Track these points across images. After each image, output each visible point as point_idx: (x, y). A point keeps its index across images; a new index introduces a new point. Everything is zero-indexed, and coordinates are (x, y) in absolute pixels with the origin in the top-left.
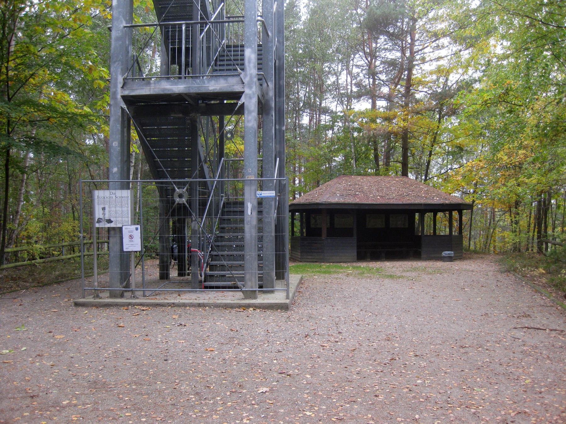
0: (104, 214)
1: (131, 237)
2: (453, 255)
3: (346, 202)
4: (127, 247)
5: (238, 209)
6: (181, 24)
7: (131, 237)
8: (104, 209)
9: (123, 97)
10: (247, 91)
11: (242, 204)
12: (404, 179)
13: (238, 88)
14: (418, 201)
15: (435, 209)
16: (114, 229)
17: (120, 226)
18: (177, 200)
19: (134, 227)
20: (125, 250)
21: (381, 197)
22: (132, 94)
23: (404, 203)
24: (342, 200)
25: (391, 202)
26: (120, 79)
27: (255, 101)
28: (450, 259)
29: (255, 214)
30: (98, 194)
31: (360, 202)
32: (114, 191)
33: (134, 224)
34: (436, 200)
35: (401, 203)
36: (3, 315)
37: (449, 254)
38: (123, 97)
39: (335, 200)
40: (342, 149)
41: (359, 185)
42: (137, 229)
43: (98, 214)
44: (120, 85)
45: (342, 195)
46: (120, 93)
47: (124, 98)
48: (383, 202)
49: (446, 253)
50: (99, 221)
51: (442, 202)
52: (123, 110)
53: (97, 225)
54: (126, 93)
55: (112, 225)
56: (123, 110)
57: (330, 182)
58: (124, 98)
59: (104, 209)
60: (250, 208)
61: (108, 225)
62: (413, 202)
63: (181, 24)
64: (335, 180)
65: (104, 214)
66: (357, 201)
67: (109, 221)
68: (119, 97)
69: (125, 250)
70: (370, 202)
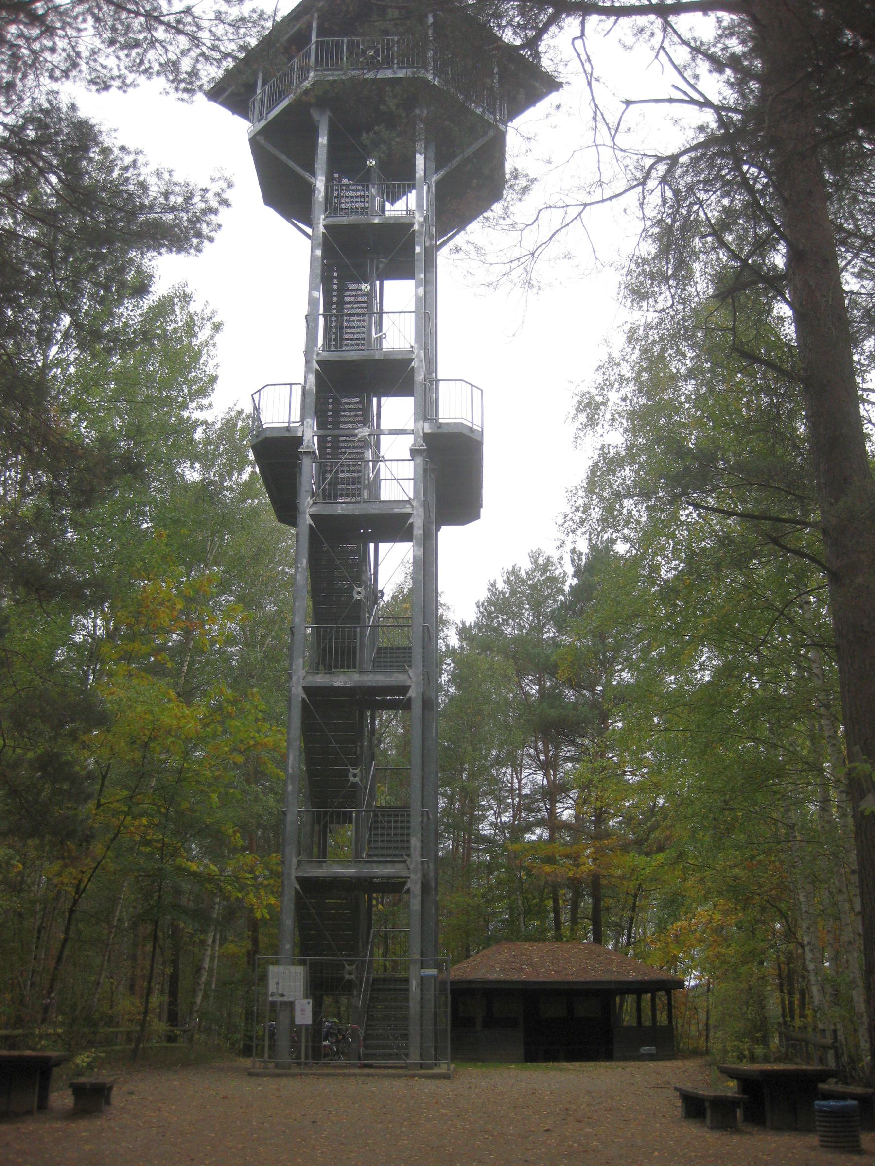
0: (277, 988)
1: (303, 1011)
2: (654, 1052)
3: (509, 979)
4: (298, 1021)
5: (404, 987)
6: (351, 813)
7: (303, 1011)
8: (277, 983)
9: (296, 878)
10: (413, 877)
11: (407, 981)
12: (595, 947)
13: (404, 873)
14: (607, 977)
15: (638, 988)
16: (285, 1003)
17: (292, 999)
18: (347, 977)
19: (307, 1001)
20: (297, 1022)
21: (557, 972)
22: (305, 875)
23: (588, 980)
24: (502, 977)
25: (571, 978)
26: (295, 861)
27: (419, 885)
28: (652, 1057)
29: (419, 990)
30: (272, 968)
31: (527, 980)
32: (288, 967)
33: (307, 998)
34: (632, 976)
35: (582, 980)
36: (4, 1127)
37: (649, 1050)
38: (296, 878)
39: (494, 977)
40: (504, 897)
41: (526, 955)
42: (309, 1003)
43: (272, 988)
44: (294, 867)
45: (503, 970)
46: (294, 874)
47: (298, 879)
48: (558, 979)
49: (645, 1049)
50: (272, 995)
51: (639, 978)
52: (296, 890)
53: (270, 999)
54: (300, 874)
55: (285, 999)
56: (296, 890)
57: (485, 952)
58: (298, 879)
59: (277, 983)
60: (414, 984)
61: (281, 999)
62: (599, 978)
63: (351, 813)
64: (494, 948)
65: (277, 988)
66: (523, 977)
67: (282, 995)
68: (293, 877)
69: (297, 1022)
70: (541, 980)
